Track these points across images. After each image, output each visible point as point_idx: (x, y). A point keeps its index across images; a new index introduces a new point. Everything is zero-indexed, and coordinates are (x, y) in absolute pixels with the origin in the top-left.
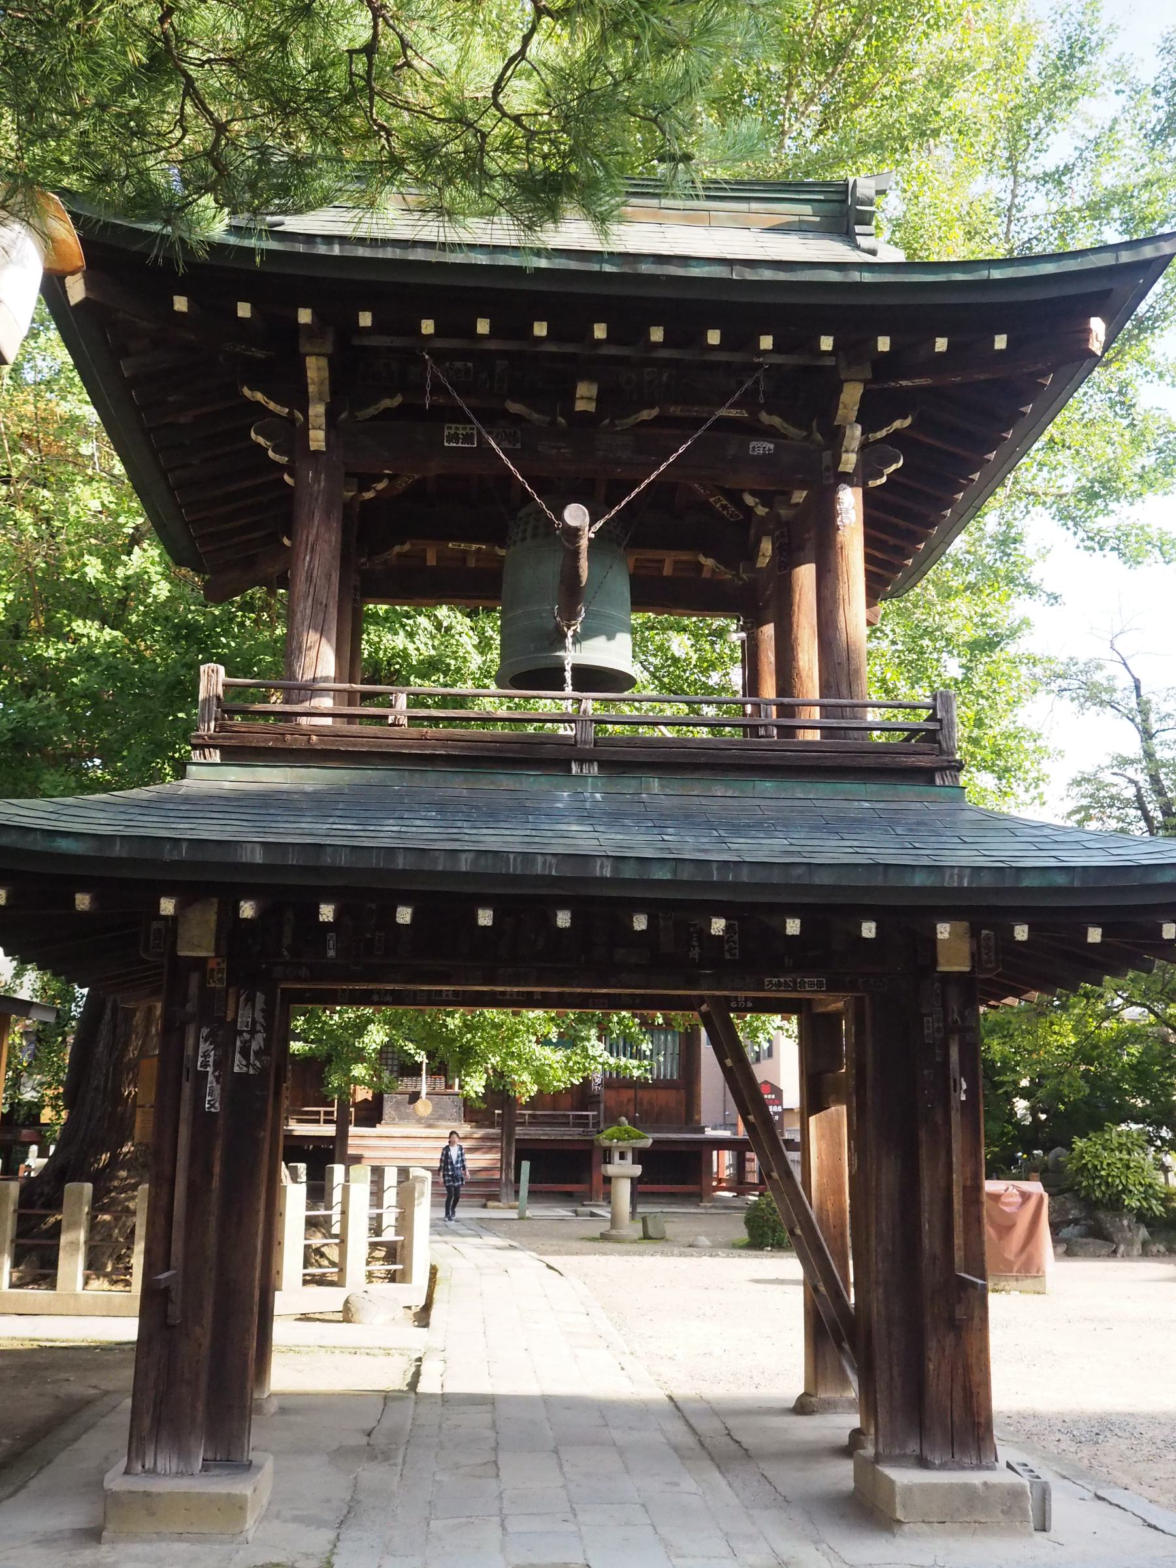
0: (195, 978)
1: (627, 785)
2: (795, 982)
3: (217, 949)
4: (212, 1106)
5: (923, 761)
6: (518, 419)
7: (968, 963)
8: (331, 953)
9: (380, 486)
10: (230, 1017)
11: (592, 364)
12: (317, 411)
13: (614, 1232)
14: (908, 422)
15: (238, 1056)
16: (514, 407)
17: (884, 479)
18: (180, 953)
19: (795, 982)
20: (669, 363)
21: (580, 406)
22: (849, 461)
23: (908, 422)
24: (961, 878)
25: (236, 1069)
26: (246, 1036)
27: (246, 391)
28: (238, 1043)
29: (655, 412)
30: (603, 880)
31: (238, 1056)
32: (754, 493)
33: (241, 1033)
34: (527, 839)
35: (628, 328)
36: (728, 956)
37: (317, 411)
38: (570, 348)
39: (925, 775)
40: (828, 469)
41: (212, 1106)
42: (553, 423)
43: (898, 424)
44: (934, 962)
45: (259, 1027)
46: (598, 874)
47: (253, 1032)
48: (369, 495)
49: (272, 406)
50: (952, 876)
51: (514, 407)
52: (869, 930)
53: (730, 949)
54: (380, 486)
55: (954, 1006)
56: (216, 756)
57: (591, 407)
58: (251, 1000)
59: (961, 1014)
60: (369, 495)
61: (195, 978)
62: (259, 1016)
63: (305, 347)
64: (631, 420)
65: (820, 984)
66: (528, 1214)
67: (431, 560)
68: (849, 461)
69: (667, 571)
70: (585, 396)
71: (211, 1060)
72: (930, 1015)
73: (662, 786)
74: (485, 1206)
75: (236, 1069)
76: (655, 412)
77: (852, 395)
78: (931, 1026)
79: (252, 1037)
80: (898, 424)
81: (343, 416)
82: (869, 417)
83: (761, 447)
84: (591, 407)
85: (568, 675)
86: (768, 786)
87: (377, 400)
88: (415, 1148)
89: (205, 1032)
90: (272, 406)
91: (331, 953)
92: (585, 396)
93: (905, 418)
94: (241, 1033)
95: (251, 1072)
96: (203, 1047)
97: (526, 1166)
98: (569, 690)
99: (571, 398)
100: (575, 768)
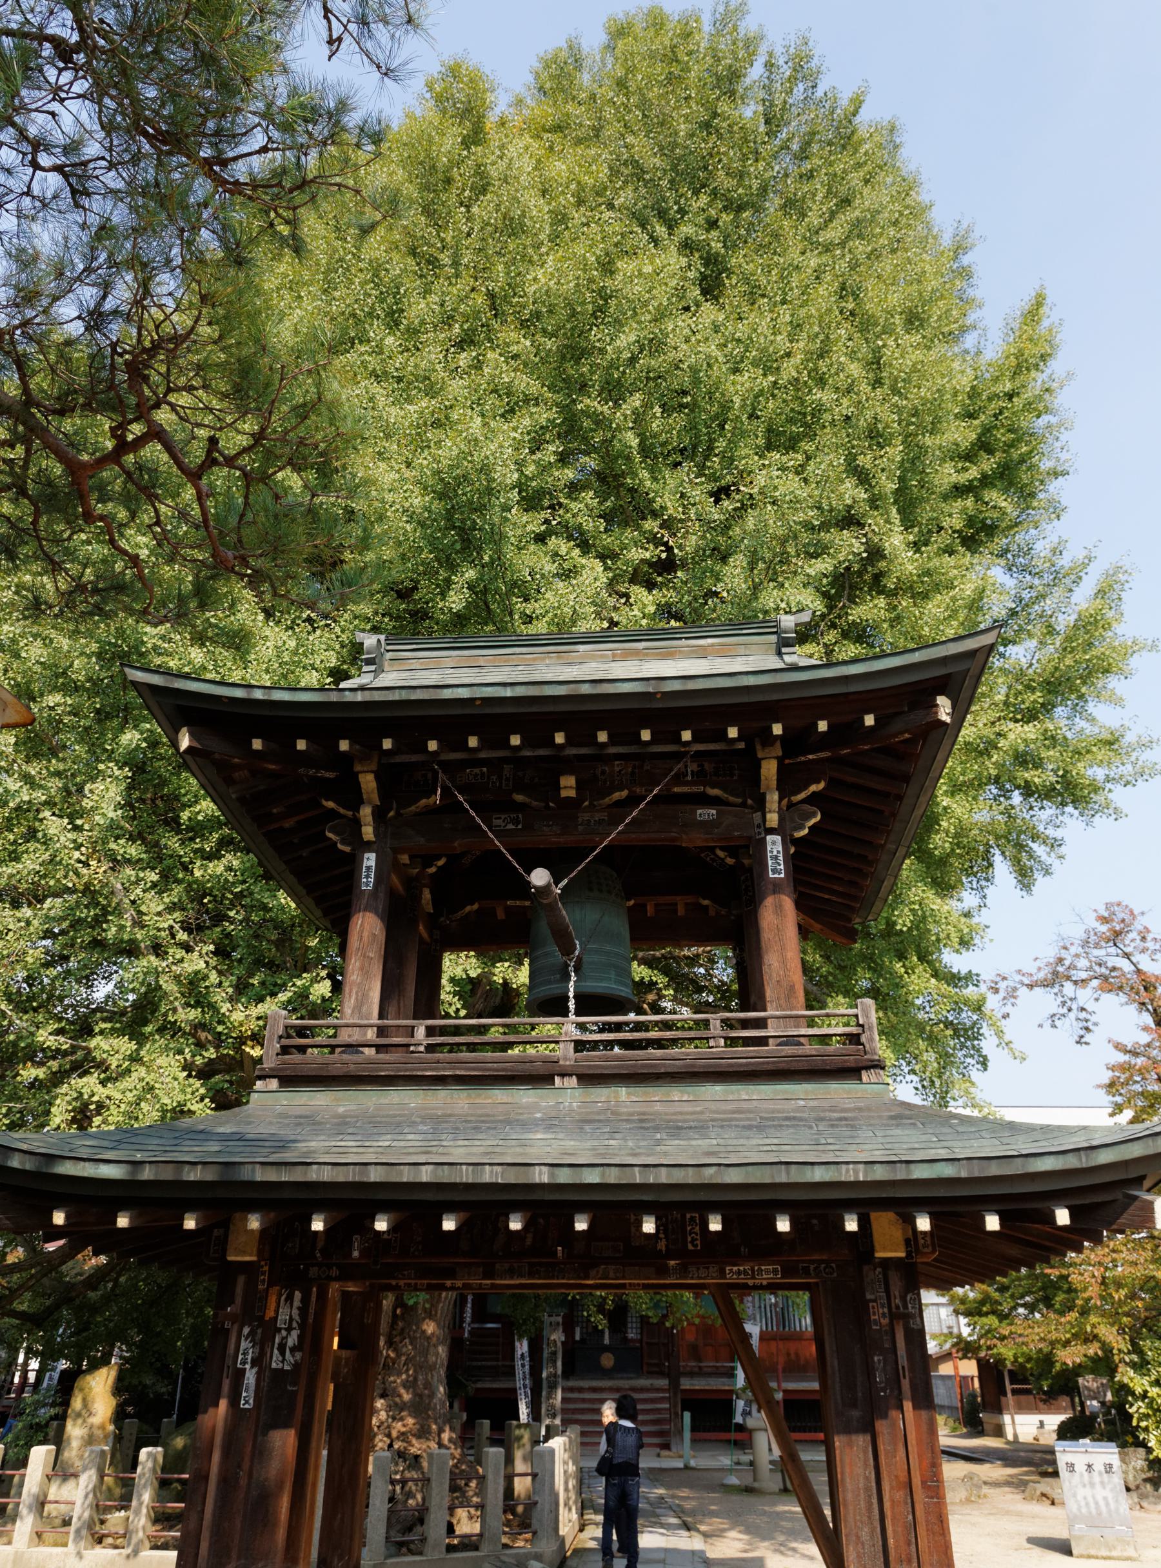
0: (241, 1280)
1: (602, 1095)
2: (753, 1270)
3: (260, 1253)
4: (247, 1402)
5: (851, 1061)
6: (522, 807)
7: (903, 1248)
8: (356, 1254)
9: (441, 863)
10: (270, 1314)
11: (560, 764)
12: (366, 812)
13: (756, 1485)
14: (822, 785)
15: (276, 1352)
16: (519, 798)
17: (806, 831)
18: (230, 1258)
19: (753, 1270)
20: (698, 754)
21: (564, 794)
22: (773, 819)
23: (822, 785)
24: (856, 1172)
25: (274, 1365)
26: (284, 1333)
27: (325, 803)
28: (277, 1341)
29: (625, 793)
30: (542, 1186)
31: (276, 1352)
32: (722, 849)
33: (279, 1330)
34: (490, 1149)
35: (666, 731)
36: (690, 1247)
37: (366, 812)
38: (583, 751)
39: (851, 1072)
40: (759, 826)
41: (247, 1402)
42: (547, 807)
43: (814, 788)
44: (872, 1250)
45: (295, 1325)
46: (537, 1181)
47: (289, 1329)
48: (433, 870)
49: (342, 811)
50: (848, 1171)
51: (519, 798)
52: (783, 1225)
53: (693, 1240)
54: (441, 863)
55: (896, 1291)
56: (274, 1084)
57: (572, 793)
58: (290, 1298)
59: (903, 1299)
60: (433, 870)
61: (241, 1280)
62: (295, 1313)
63: (358, 768)
64: (607, 800)
65: (775, 1271)
66: (693, 1463)
67: (501, 915)
68: (773, 819)
69: (681, 911)
70: (568, 785)
71: (249, 1357)
72: (875, 1301)
73: (628, 1094)
74: (659, 1455)
75: (274, 1365)
76: (625, 793)
77: (769, 769)
79: (289, 1333)
80: (814, 788)
81: (392, 814)
82: (788, 782)
83: (707, 813)
84: (572, 793)
85: (572, 1005)
86: (716, 1091)
87: (806, 787)
88: (584, 1400)
89: (246, 1330)
90: (342, 811)
91: (356, 1254)
92: (568, 785)
93: (819, 782)
94: (279, 1330)
95: (287, 1367)
96: (244, 1344)
97: (687, 1416)
98: (572, 1017)
99: (558, 788)
100: (557, 1079)
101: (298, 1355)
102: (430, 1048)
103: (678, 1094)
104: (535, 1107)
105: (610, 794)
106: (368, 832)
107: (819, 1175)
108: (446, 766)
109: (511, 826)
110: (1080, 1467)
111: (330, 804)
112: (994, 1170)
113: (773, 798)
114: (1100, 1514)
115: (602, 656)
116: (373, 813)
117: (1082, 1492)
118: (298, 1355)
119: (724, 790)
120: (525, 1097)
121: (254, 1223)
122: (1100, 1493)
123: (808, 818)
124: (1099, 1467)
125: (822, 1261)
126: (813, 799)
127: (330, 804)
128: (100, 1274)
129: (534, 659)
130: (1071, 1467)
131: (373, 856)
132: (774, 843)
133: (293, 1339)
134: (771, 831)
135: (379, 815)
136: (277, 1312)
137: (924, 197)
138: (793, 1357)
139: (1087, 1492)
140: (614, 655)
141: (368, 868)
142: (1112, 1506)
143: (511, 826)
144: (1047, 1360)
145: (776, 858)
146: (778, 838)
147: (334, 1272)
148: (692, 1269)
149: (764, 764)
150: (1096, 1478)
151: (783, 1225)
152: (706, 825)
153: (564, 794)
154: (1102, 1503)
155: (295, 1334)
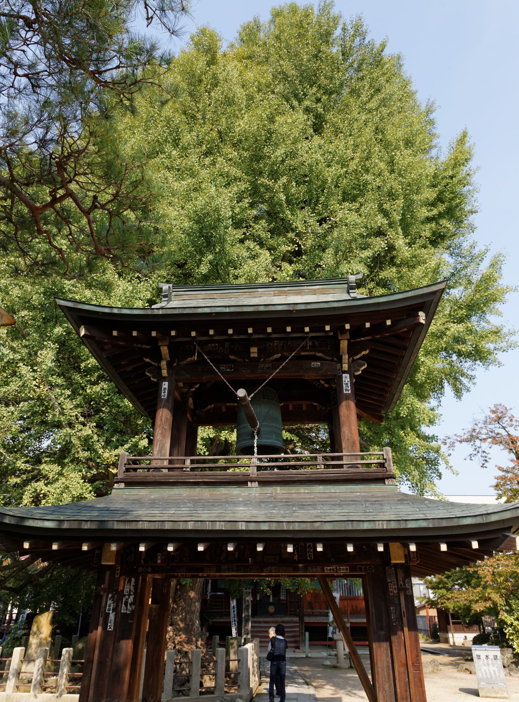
0: (108, 573)
1: (269, 490)
2: (336, 569)
3: (116, 561)
4: (110, 628)
5: (380, 475)
6: (233, 361)
7: (404, 559)
8: (159, 561)
9: (197, 386)
10: (121, 588)
11: (250, 342)
12: (164, 364)
13: (338, 665)
14: (367, 352)
15: (123, 605)
16: (232, 357)
17: (360, 372)
18: (103, 563)
19: (336, 569)
20: (312, 338)
21: (252, 355)
22: (345, 367)
23: (367, 352)
24: (383, 525)
25: (122, 611)
26: (127, 597)
27: (145, 359)
28: (124, 600)
29: (279, 355)
30: (242, 531)
31: (123, 605)
32: (323, 380)
33: (125, 595)
34: (219, 515)
35: (298, 327)
36: (309, 558)
37: (164, 364)
38: (261, 336)
39: (380, 480)
40: (339, 370)
41: (110, 628)
42: (245, 361)
43: (364, 353)
44: (390, 560)
45: (132, 593)
46: (240, 529)
47: (129, 595)
48: (193, 389)
49: (153, 363)
50: (379, 524)
51: (232, 357)
52: (350, 548)
53: (310, 555)
54: (197, 386)
55: (400, 578)
56: (122, 485)
57: (256, 355)
58: (130, 581)
59: (404, 581)
60: (193, 389)
61: (108, 573)
62: (132, 588)
63: (160, 344)
64: (271, 358)
65: (346, 569)
66: (310, 655)
67: (224, 410)
68: (345, 367)
69: (304, 408)
70: (254, 351)
71: (111, 608)
72: (391, 582)
73: (281, 490)
74: (294, 652)
75: (122, 611)
76: (279, 355)
77: (344, 344)
78: (393, 589)
79: (129, 597)
80: (364, 353)
81: (175, 364)
82: (352, 350)
83: (316, 364)
84: (256, 355)
86: (320, 488)
87: (360, 352)
88: (261, 627)
89: (110, 596)
90: (153, 363)
91: (159, 561)
92: (254, 351)
93: (366, 350)
94: (125, 595)
95: (128, 612)
96: (109, 602)
97: (307, 634)
99: (249, 353)
100: (249, 483)
101: (133, 607)
102: (192, 469)
103: (303, 490)
104: (239, 496)
105: (273, 355)
106: (165, 373)
107: (366, 526)
108: (199, 343)
109: (228, 370)
110: (483, 657)
111: (148, 360)
112: (444, 524)
113: (345, 357)
114: (492, 678)
115: (269, 294)
116: (167, 364)
117: (483, 668)
118: (133, 607)
119: (324, 354)
120: (235, 491)
121: (114, 547)
122: (492, 668)
123: (361, 366)
124: (491, 657)
125: (368, 565)
126: (363, 358)
127: (148, 360)
128: (45, 570)
129: (239, 295)
130: (479, 657)
131: (167, 383)
132: (346, 377)
133: (131, 600)
134: (345, 372)
135: (169, 365)
136: (124, 587)
137: (413, 88)
138: (354, 607)
139: (486, 668)
140: (274, 293)
141: (165, 389)
142: (497, 674)
143: (228, 370)
144: (468, 609)
145: (347, 384)
146: (348, 375)
147: (150, 569)
148: (309, 568)
149: (342, 342)
150: (490, 662)
151: (350, 548)
152: (316, 369)
153: (252, 355)
154: (493, 673)
155: (132, 597)
